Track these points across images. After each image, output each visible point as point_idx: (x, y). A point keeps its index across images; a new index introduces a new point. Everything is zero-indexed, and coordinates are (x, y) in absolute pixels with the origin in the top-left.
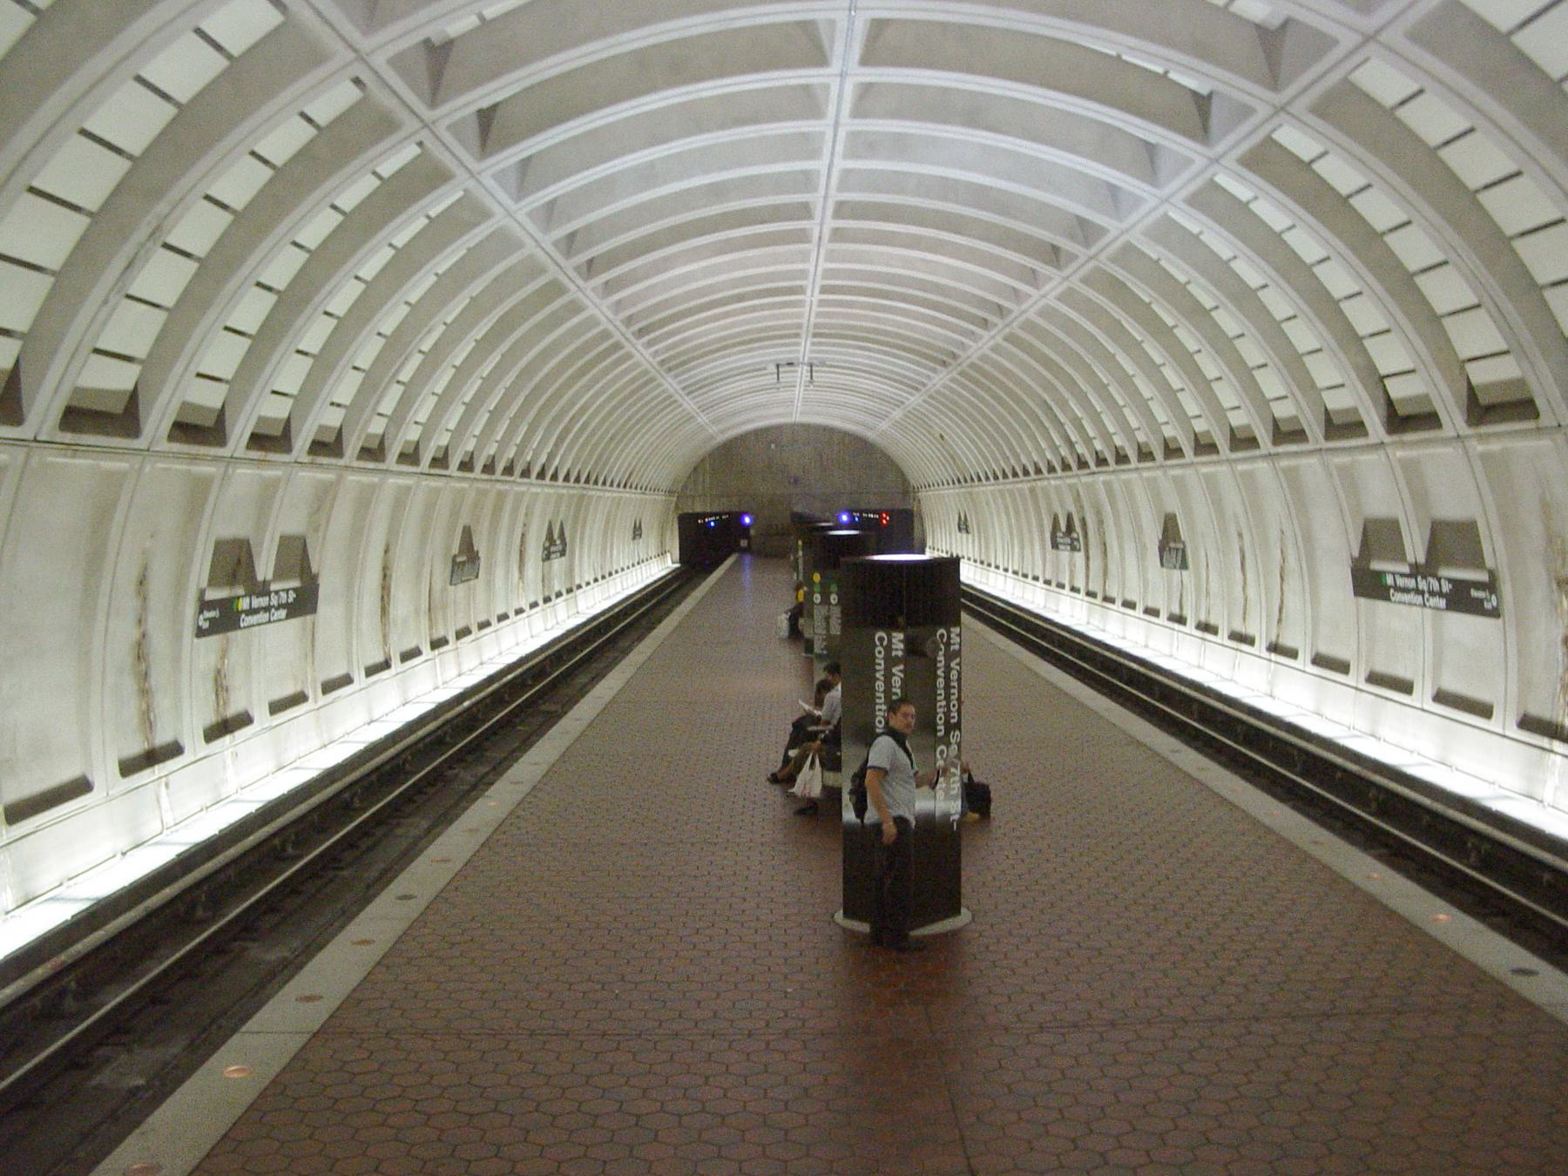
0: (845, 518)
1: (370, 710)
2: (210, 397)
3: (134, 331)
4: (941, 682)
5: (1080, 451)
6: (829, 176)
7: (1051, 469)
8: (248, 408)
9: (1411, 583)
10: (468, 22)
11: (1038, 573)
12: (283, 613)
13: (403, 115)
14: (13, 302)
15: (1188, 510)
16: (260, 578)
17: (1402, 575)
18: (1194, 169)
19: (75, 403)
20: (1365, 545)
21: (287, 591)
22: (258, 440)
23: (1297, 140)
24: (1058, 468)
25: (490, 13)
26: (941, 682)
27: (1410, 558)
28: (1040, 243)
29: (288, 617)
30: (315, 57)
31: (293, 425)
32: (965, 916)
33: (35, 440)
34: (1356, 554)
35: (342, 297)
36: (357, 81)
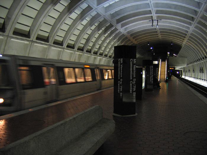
4: (131, 69)
5: (199, 58)
7: (201, 59)
10: (114, 2)
11: (203, 79)
14: (3, 14)
15: (204, 67)
19: (15, 31)
22: (87, 51)
24: (204, 58)
25: (116, 1)
26: (131, 69)
28: (185, 33)
30: (91, 9)
31: (75, 45)
32: (136, 114)
33: (33, 41)
35: (94, 40)
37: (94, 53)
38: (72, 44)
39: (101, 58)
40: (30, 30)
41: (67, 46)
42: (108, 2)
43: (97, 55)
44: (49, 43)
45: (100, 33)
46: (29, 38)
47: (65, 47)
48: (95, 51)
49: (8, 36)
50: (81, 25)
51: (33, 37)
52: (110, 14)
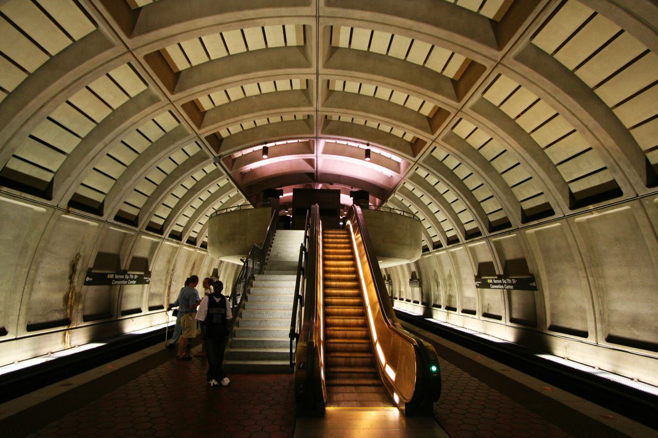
0: (341, 223)
1: (151, 322)
2: (195, 235)
3: (183, 221)
6: (317, 82)
8: (169, 227)
9: (500, 281)
12: (135, 282)
13: (162, 98)
16: (123, 268)
17: (496, 279)
18: (441, 137)
20: (479, 272)
21: (134, 275)
23: (422, 173)
27: (497, 273)
29: (136, 283)
34: (476, 274)
36: (227, 179)
37: (188, 242)
38: (159, 225)
39: (191, 249)
40: (52, 180)
41: (188, 240)
42: (424, 192)
43: (196, 247)
44: (53, 200)
45: (221, 186)
46: (101, 215)
47: (167, 237)
48: (190, 237)
49: (164, 239)
50: (202, 171)
51: (62, 196)
52: (373, 169)
